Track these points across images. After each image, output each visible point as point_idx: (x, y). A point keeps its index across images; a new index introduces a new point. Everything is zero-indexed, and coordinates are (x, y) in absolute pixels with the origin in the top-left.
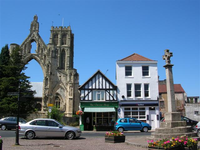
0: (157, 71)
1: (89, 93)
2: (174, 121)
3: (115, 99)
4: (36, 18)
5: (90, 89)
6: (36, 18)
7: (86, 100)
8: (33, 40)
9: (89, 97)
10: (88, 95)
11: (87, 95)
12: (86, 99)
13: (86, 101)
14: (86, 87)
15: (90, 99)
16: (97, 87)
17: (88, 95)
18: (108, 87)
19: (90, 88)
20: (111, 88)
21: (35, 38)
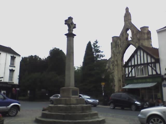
0: (53, 49)
1: (132, 69)
2: (81, 104)
3: (159, 73)
4: (127, 9)
5: (133, 66)
6: (127, 9)
7: (130, 77)
8: (128, 30)
9: (133, 73)
10: (131, 71)
11: (130, 72)
12: (130, 75)
13: (130, 78)
14: (130, 64)
15: (134, 75)
16: (136, 63)
17: (131, 71)
18: (149, 61)
19: (133, 64)
20: (153, 61)
21: (129, 26)
